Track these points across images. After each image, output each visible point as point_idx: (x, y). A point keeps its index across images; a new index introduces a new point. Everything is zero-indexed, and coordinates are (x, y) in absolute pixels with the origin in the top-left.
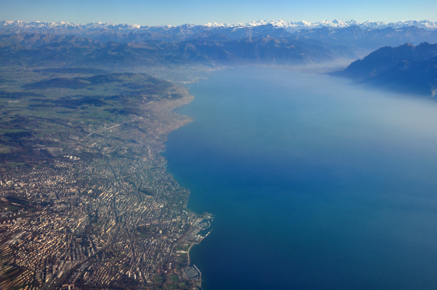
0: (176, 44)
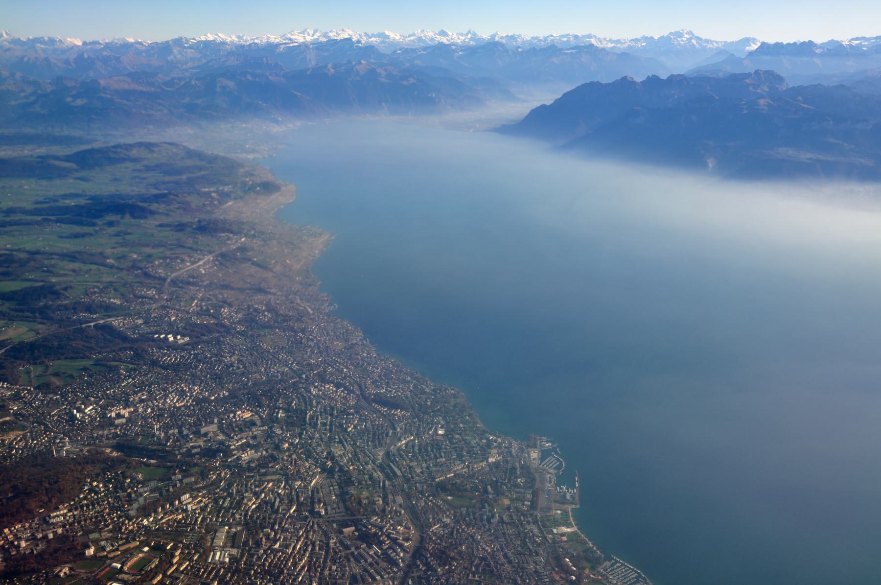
0: (196, 80)
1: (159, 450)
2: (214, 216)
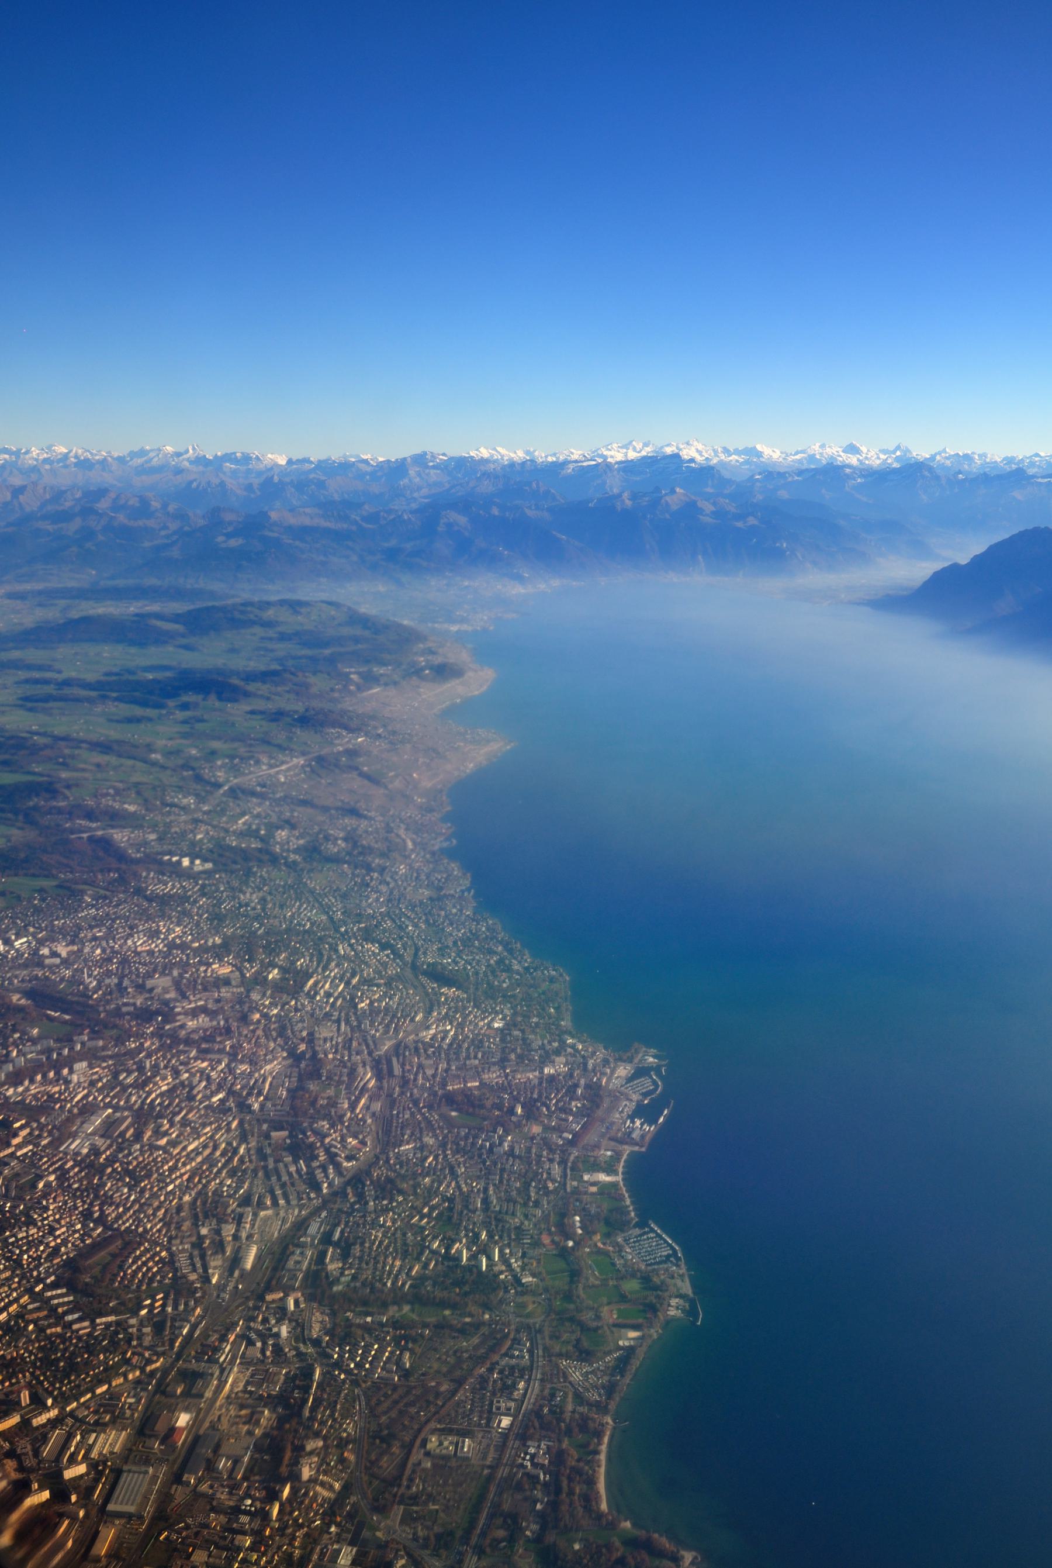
1: (78, 1003)
2: (339, 706)
